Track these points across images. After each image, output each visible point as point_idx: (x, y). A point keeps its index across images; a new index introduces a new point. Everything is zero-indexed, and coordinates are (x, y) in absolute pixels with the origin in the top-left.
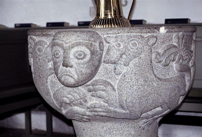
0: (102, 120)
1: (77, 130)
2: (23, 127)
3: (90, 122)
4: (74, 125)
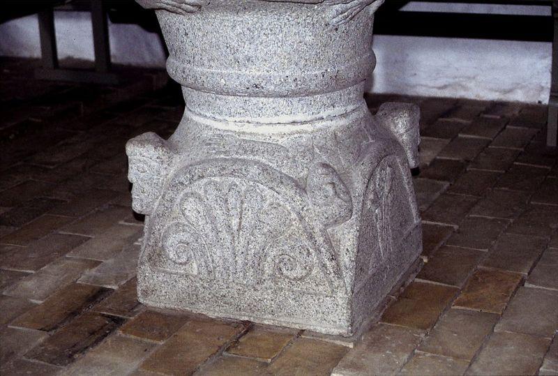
0: (230, 6)
1: (169, 37)
2: (37, 53)
3: (201, 14)
4: (162, 24)
